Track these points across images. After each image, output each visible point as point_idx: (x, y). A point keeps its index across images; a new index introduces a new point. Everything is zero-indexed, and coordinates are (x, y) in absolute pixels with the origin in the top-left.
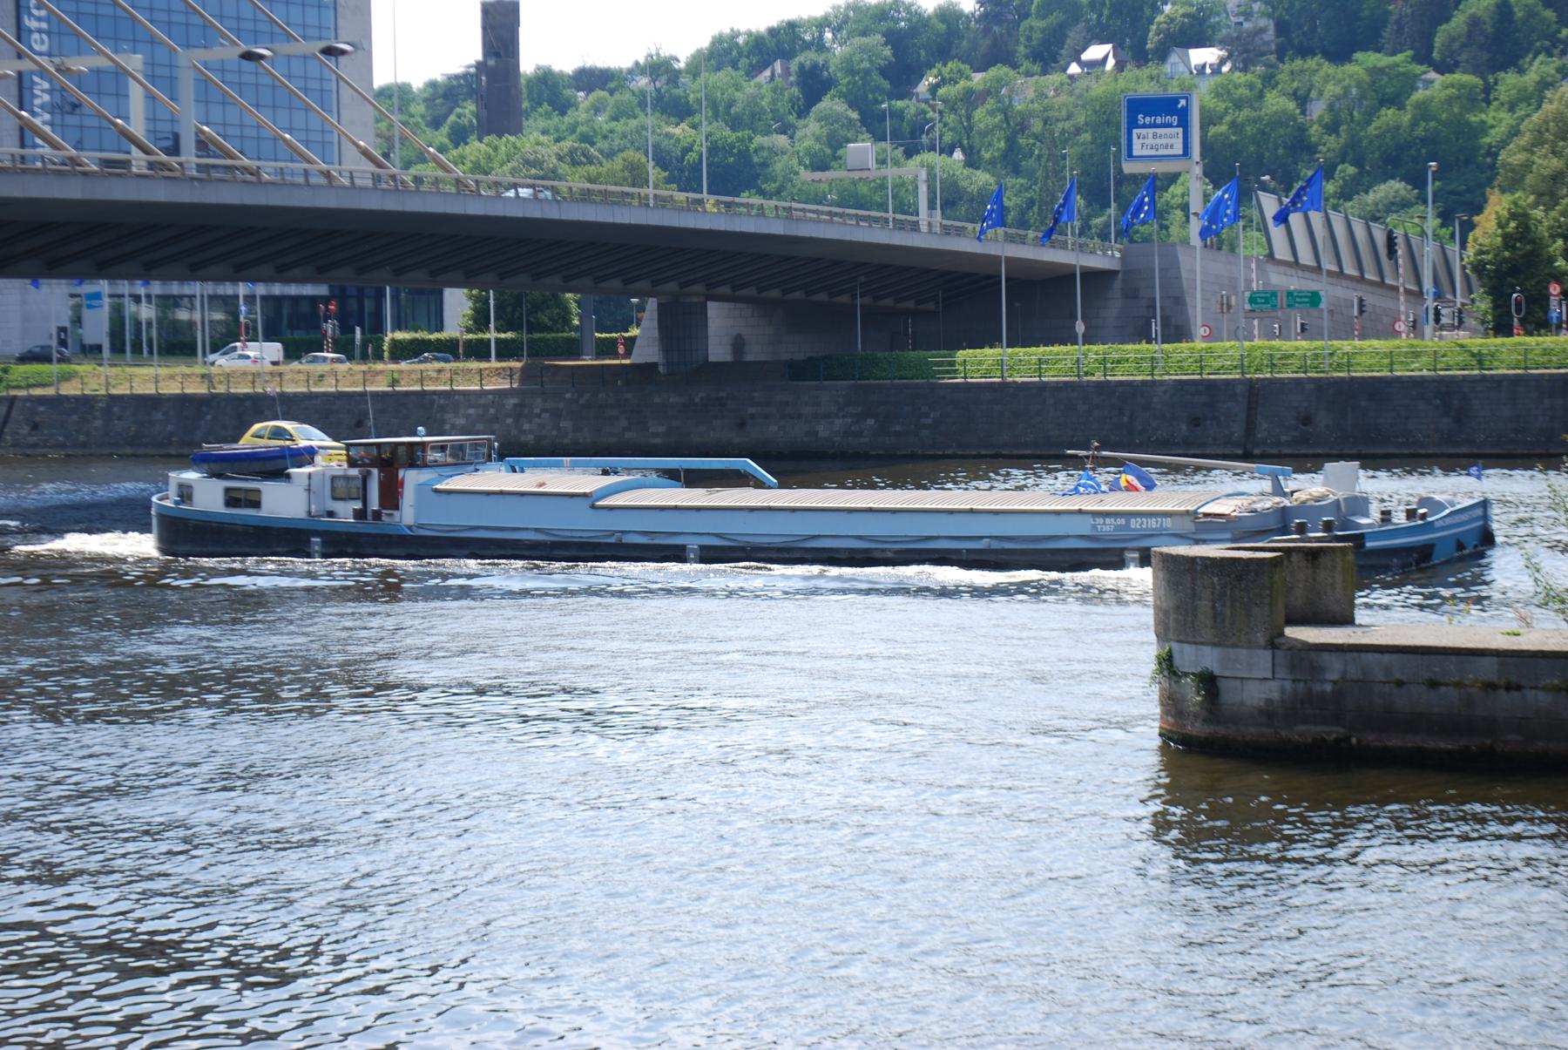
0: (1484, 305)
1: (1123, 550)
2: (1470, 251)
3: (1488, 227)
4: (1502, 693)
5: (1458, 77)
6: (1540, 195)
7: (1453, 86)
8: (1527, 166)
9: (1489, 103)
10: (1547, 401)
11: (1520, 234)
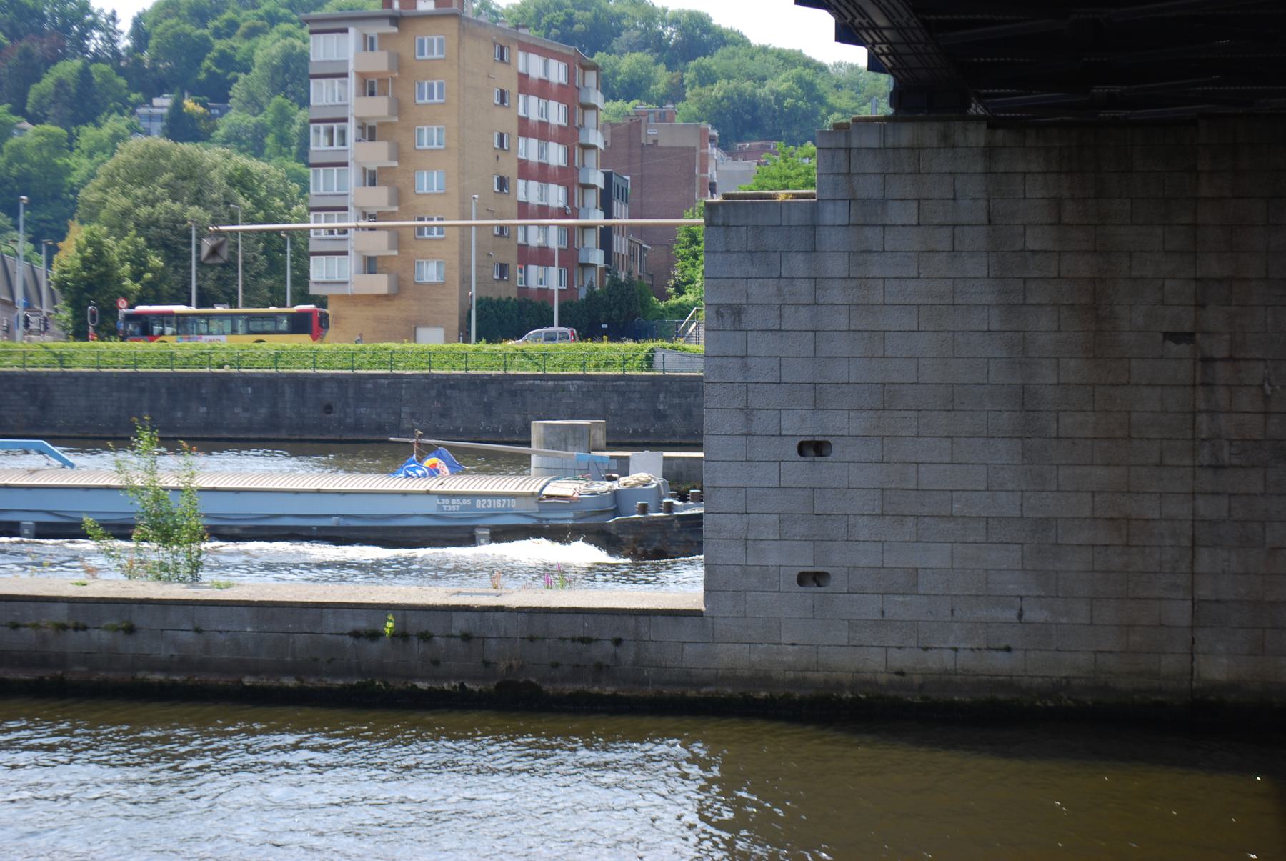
0: (66, 314)
1: (474, 527)
2: (55, 273)
3: (70, 253)
4: (71, 633)
5: (48, 127)
6: (111, 227)
7: (43, 135)
8: (102, 203)
9: (71, 149)
10: (115, 394)
11: (96, 258)
